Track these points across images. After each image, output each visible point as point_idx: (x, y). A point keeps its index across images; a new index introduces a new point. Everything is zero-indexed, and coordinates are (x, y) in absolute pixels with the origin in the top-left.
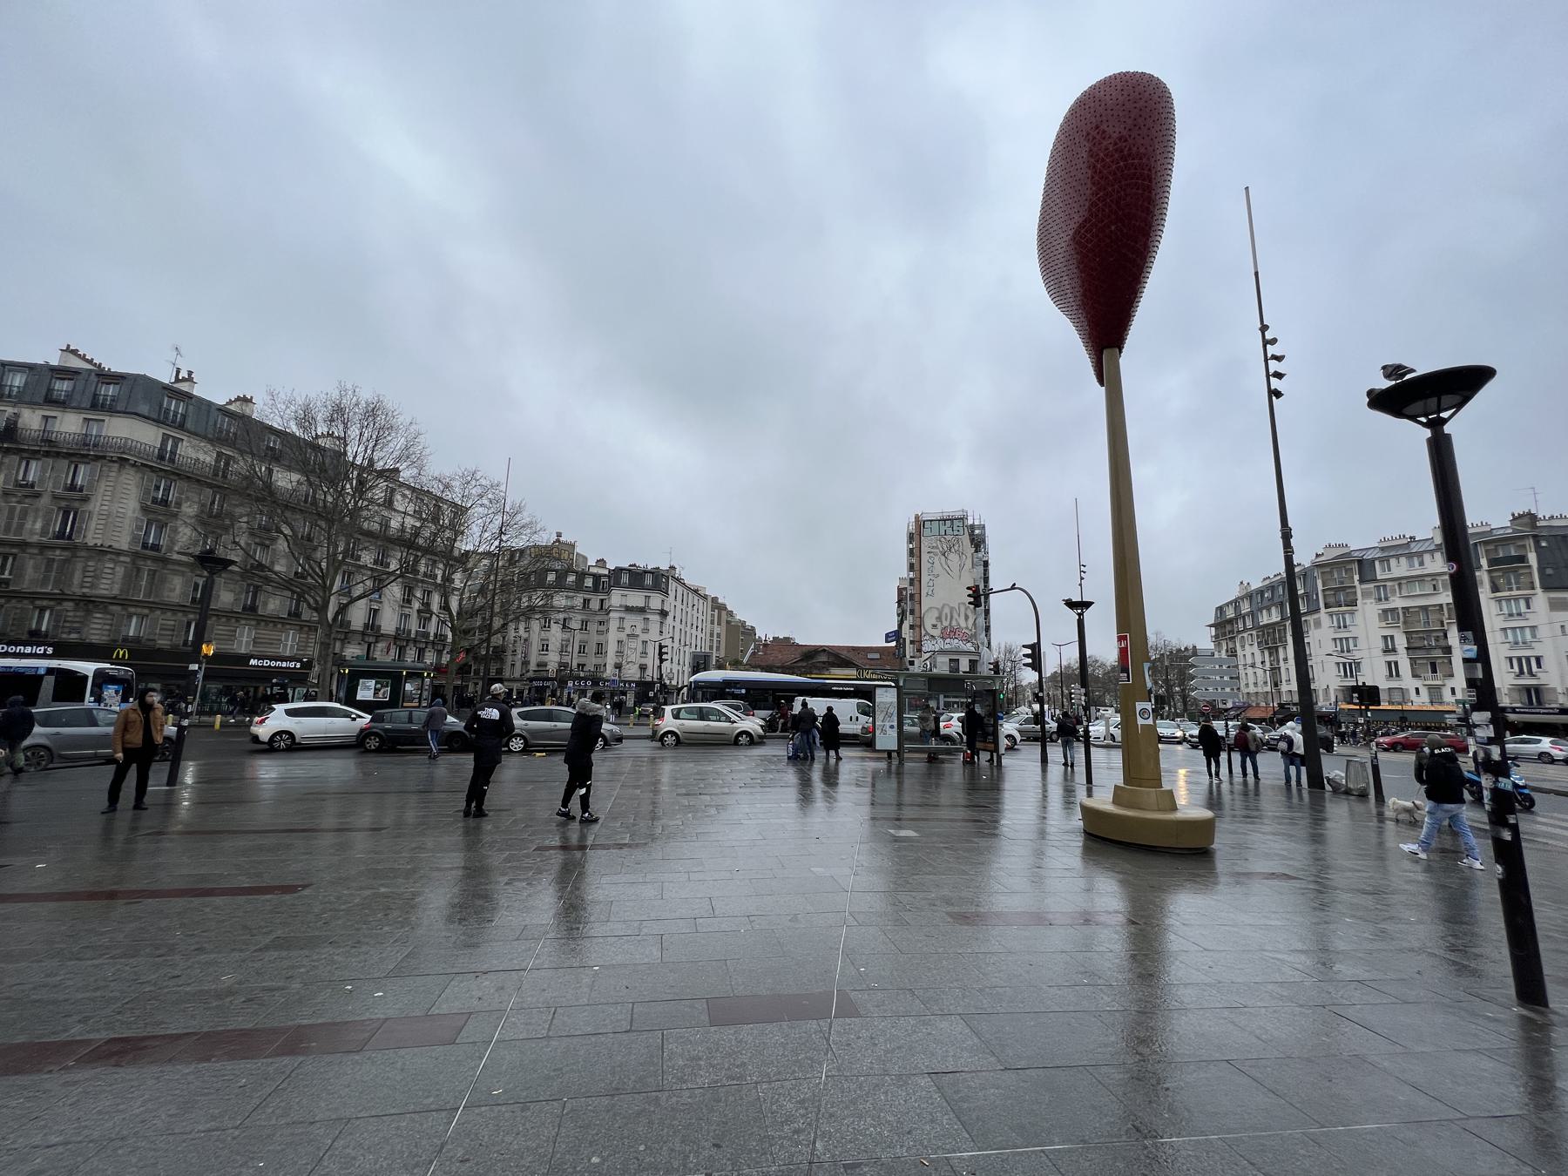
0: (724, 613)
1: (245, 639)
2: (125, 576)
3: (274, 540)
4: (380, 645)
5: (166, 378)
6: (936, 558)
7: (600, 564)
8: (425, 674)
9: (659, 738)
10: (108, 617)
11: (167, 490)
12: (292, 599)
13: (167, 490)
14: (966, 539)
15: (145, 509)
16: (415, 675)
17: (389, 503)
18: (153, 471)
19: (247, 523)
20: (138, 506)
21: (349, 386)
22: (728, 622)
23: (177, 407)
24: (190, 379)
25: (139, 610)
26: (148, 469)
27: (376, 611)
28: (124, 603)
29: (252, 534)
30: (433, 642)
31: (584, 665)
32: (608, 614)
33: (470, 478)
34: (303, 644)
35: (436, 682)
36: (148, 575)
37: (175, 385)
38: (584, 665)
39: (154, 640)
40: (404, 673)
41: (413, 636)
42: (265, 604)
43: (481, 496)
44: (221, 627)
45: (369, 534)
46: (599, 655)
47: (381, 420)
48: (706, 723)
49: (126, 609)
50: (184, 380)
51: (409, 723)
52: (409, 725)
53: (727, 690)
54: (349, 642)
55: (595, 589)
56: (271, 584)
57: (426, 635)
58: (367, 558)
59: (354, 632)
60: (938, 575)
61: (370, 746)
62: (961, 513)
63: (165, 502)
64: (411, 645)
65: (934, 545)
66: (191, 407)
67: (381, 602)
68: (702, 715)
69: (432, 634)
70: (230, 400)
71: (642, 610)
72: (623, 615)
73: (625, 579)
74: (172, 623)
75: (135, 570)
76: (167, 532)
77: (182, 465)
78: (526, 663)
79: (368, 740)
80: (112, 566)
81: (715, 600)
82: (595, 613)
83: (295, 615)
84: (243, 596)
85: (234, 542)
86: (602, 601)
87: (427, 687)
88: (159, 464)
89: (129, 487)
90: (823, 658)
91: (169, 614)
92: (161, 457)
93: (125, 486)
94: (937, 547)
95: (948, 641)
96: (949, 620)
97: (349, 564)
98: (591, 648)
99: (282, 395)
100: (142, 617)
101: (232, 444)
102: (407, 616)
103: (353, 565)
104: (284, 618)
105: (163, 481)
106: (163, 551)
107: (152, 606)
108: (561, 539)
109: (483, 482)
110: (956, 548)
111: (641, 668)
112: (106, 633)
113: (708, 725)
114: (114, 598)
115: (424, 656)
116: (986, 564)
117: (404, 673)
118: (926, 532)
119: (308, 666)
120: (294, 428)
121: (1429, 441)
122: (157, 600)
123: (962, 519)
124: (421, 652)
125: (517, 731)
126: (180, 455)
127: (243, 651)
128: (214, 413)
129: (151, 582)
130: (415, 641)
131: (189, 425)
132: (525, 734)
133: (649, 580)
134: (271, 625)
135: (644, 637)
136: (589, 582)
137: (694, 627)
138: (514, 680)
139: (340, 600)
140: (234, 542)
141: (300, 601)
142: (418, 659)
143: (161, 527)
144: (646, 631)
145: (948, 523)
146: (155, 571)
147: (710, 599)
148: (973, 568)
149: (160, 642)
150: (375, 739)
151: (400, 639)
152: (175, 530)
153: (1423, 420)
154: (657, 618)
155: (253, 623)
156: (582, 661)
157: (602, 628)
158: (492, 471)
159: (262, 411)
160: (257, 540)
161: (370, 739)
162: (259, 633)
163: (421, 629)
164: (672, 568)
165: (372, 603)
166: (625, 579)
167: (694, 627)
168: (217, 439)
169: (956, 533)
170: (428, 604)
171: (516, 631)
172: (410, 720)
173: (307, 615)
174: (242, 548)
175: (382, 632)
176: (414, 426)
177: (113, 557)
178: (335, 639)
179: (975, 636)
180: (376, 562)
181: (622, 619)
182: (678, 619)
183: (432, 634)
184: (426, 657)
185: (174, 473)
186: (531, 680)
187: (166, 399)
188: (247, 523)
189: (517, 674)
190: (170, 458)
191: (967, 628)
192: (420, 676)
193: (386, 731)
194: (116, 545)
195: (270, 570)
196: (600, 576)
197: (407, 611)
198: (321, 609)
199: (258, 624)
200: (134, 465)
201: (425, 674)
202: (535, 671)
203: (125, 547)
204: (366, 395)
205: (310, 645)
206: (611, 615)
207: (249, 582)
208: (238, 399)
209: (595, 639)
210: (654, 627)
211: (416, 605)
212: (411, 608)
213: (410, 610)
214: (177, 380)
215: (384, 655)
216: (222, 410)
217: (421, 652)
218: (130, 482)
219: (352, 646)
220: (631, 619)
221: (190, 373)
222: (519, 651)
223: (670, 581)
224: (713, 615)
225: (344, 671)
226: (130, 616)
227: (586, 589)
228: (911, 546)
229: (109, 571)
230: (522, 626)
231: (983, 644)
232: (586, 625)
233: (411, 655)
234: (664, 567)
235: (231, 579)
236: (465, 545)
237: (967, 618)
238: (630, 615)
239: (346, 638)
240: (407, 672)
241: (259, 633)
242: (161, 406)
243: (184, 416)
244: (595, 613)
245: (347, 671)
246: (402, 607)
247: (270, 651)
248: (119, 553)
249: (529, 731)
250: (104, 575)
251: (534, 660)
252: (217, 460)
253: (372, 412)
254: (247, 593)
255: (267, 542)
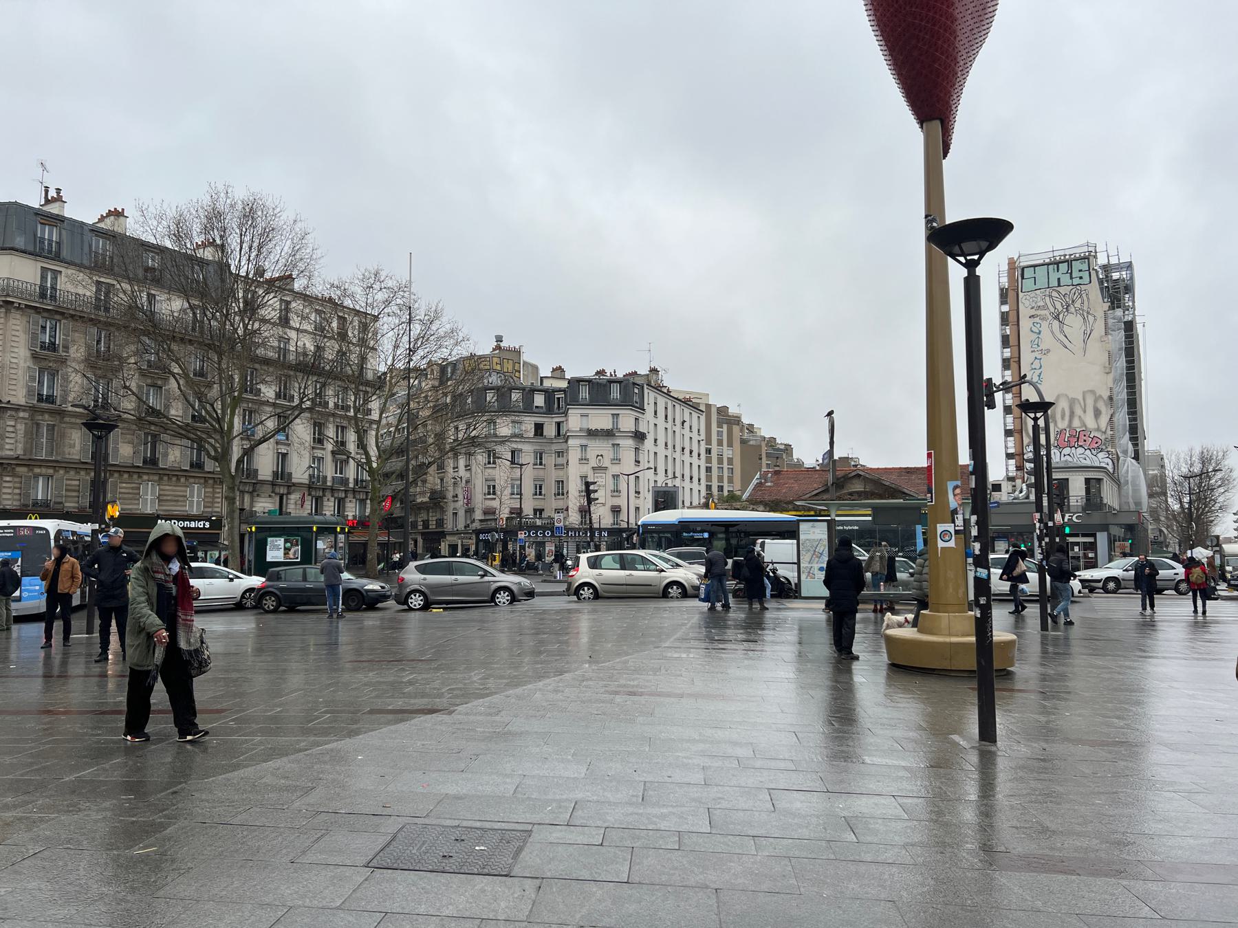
0: (736, 429)
1: (149, 497)
2: (26, 432)
3: (166, 380)
4: (295, 497)
5: (34, 200)
6: (1045, 324)
7: (558, 374)
8: (338, 529)
9: (576, 591)
10: (17, 480)
11: (54, 329)
12: (192, 448)
13: (54, 329)
14: (1094, 291)
15: (35, 356)
16: (327, 530)
17: (284, 321)
18: (39, 313)
19: (135, 363)
20: (28, 354)
21: (221, 188)
22: (743, 442)
23: (51, 234)
24: (59, 199)
25: (44, 471)
26: (33, 311)
27: (284, 455)
28: (30, 463)
29: (143, 374)
30: (354, 491)
31: (541, 511)
32: (566, 442)
33: (373, 280)
34: (210, 500)
35: (354, 538)
36: (48, 430)
37: (44, 208)
38: (541, 511)
39: (61, 503)
40: (315, 529)
41: (329, 484)
42: (166, 455)
43: (387, 303)
44: (124, 485)
45: (266, 362)
46: (561, 497)
47: (261, 224)
48: (628, 572)
49: (32, 470)
50: (54, 200)
51: (303, 581)
52: (303, 583)
53: (685, 534)
54: (258, 495)
55: (549, 409)
56: (168, 432)
57: (345, 481)
58: (269, 392)
59: (263, 482)
60: (1048, 351)
61: (268, 607)
62: (1085, 249)
63: (52, 346)
64: (328, 494)
65: (1041, 304)
66: (64, 232)
67: (289, 445)
68: (624, 564)
69: (351, 480)
70: (102, 215)
71: (608, 434)
72: (584, 442)
73: (584, 393)
74: (77, 483)
75: (35, 426)
76: (58, 381)
77: (64, 302)
78: (470, 511)
79: (264, 602)
80: (12, 423)
81: (722, 411)
82: (550, 441)
83: (197, 466)
84: (142, 448)
85: (125, 387)
86: (558, 424)
87: (341, 545)
88: (42, 303)
89: (17, 334)
90: (858, 487)
91: (72, 473)
92: (43, 295)
93: (14, 333)
94: (1045, 307)
95: (1067, 451)
96: (1067, 418)
97: (248, 401)
98: (550, 488)
99: (151, 209)
100: (48, 477)
101: (110, 271)
102: (320, 459)
103: (253, 401)
104: (186, 471)
105: (48, 323)
106: (58, 403)
107: (56, 465)
108: (502, 344)
109: (390, 284)
110: (1078, 305)
111: (613, 511)
112: (17, 497)
113: (631, 575)
114: (17, 458)
115: (344, 507)
116: (1129, 327)
117: (315, 529)
118: (1028, 284)
119: (217, 525)
120: (168, 244)
121: (966, 279)
122: (59, 458)
123: (1087, 258)
124: (341, 503)
125: (413, 587)
126: (60, 290)
127: (149, 511)
128: (88, 235)
129: (51, 439)
130: (332, 490)
131: (65, 253)
132: (423, 589)
133: (615, 393)
134: (174, 479)
135: (615, 469)
136: (539, 400)
137: (687, 451)
138: (458, 533)
139: (242, 445)
140: (125, 387)
141: (201, 451)
142: (339, 512)
143: (53, 375)
144: (616, 460)
145: (1063, 267)
146: (54, 425)
147: (714, 411)
148: (1106, 334)
149: (67, 504)
150: (270, 599)
151: (316, 488)
152: (66, 380)
153: (962, 259)
154: (630, 443)
155: (156, 478)
156: (539, 505)
157: (560, 460)
158: (396, 272)
159: (134, 227)
160: (149, 381)
161: (266, 600)
162: (163, 490)
163: (338, 475)
164: (654, 371)
165: (279, 446)
166: (584, 393)
167: (687, 451)
168: (97, 266)
169: (1076, 281)
170: (343, 443)
171: (457, 468)
172: (305, 579)
173: (210, 465)
174: (133, 393)
175: (293, 481)
176: (299, 225)
177: (13, 413)
178: (242, 492)
179: (1112, 441)
180: (278, 396)
181: (584, 447)
182: (661, 442)
183: (351, 480)
184: (347, 509)
185: (57, 312)
186: (478, 532)
187: (39, 226)
188: (135, 363)
189: (461, 526)
190: (51, 296)
191: (1098, 429)
192: (333, 531)
193: (281, 589)
194: (13, 400)
195: (165, 417)
196: (555, 390)
197: (319, 453)
198: (222, 457)
199: (161, 479)
200: (18, 308)
201: (338, 529)
202: (481, 521)
203: (22, 401)
204: (240, 194)
205: (217, 495)
206: (571, 442)
207: (146, 431)
208: (110, 213)
209: (553, 475)
210: (628, 456)
211: (329, 447)
212: (324, 449)
213: (322, 452)
214: (48, 202)
215: (299, 508)
216: (95, 231)
217: (341, 503)
218: (18, 328)
219: (263, 500)
220: (598, 448)
221: (58, 191)
222: (460, 497)
223: (646, 391)
224: (720, 434)
225: (251, 528)
226: (36, 476)
227: (536, 410)
228: (1006, 308)
229: (11, 429)
230: (462, 462)
231: (1125, 452)
232: (541, 459)
233: (329, 508)
234: (643, 370)
235: (128, 429)
236: (379, 365)
237: (1097, 414)
238: (593, 441)
239: (254, 490)
240: (318, 528)
241: (163, 490)
242: (35, 235)
243: (59, 244)
244: (550, 441)
245: (254, 529)
246: (313, 448)
247: (177, 509)
248: (17, 408)
249: (429, 586)
250: (7, 435)
251: (479, 502)
252: (98, 291)
253: (249, 214)
254: (146, 444)
255: (159, 383)
